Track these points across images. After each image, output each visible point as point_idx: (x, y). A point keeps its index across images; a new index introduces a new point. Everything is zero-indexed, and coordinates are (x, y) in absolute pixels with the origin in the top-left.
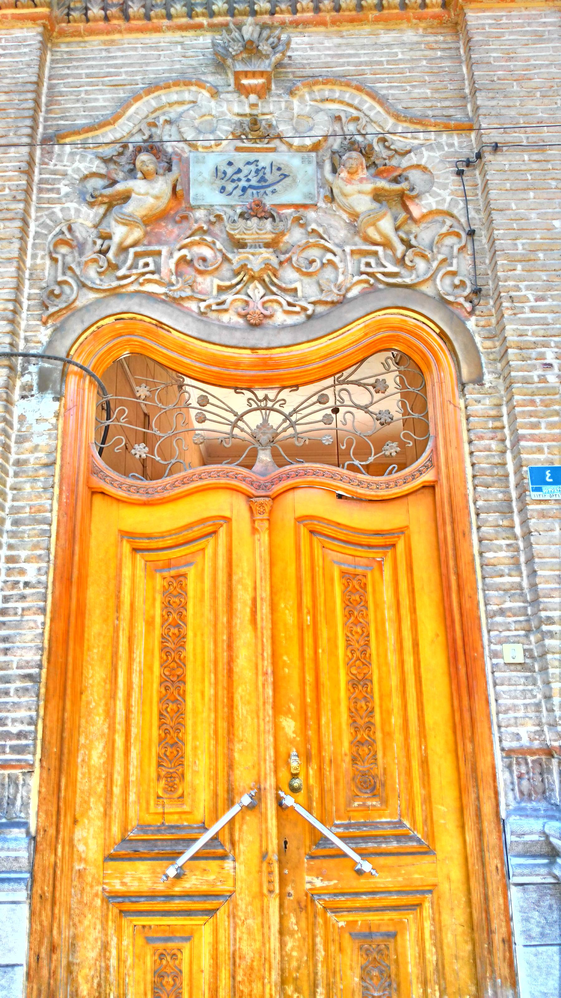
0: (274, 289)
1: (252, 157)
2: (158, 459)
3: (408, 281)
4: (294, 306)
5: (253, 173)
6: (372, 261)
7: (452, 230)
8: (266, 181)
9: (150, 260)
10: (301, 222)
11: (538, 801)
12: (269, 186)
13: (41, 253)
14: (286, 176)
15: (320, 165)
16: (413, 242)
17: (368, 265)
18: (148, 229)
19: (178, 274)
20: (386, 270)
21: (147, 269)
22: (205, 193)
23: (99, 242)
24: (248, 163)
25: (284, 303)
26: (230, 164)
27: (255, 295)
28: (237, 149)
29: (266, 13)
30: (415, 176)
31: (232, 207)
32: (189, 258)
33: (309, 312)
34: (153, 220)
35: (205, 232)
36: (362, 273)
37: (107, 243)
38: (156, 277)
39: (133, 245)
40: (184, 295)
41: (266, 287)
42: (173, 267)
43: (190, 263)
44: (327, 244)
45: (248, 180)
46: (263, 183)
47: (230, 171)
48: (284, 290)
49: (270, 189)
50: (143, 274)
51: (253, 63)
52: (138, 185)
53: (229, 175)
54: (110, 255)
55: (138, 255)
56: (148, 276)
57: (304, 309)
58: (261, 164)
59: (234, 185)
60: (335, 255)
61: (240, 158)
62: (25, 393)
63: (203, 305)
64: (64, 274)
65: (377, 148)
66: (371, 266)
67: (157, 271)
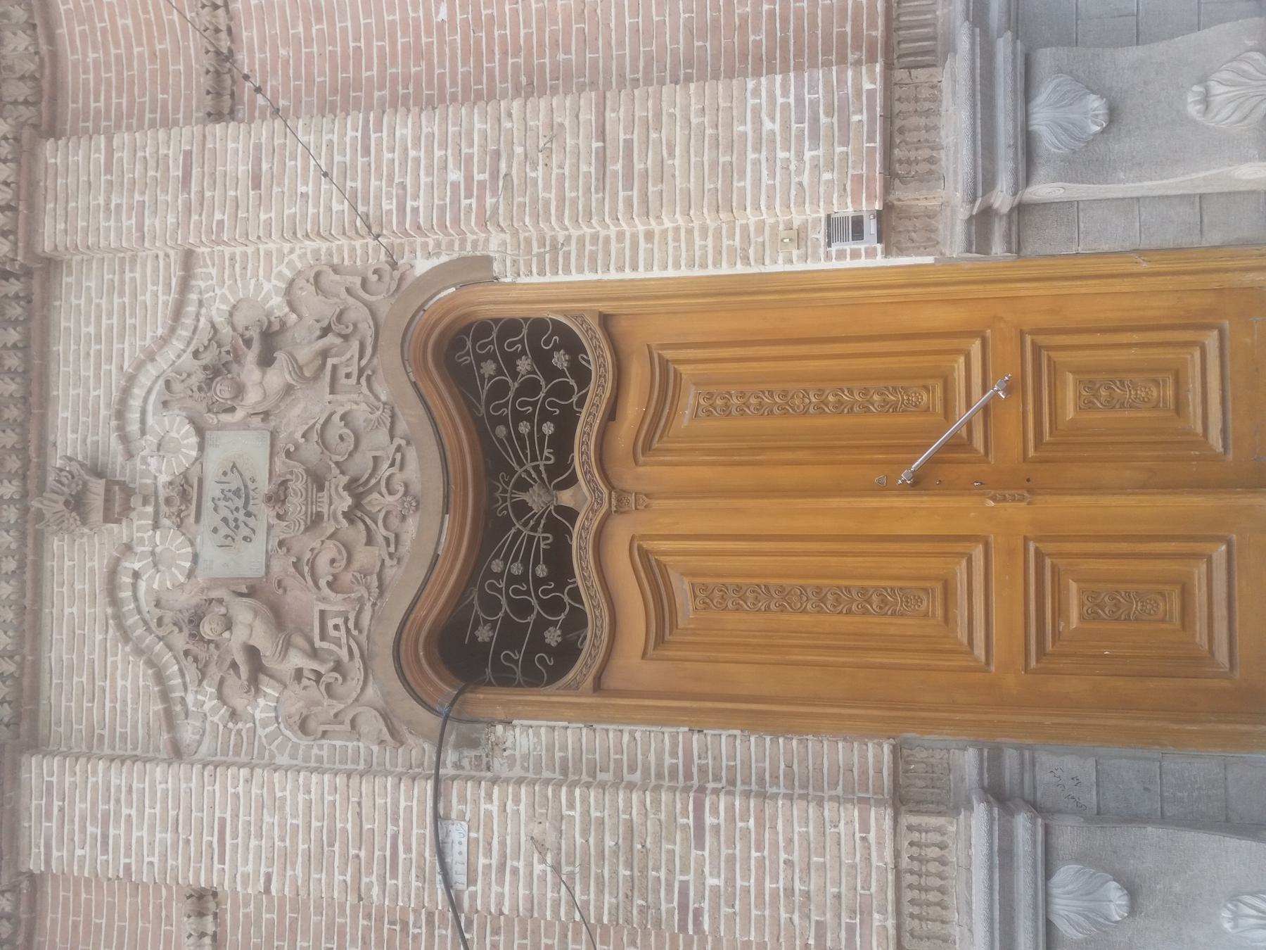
2: (563, 616)
3: (370, 333)
4: (394, 460)
7: (312, 280)
8: (239, 490)
9: (331, 623)
10: (292, 449)
12: (246, 487)
14: (234, 466)
15: (221, 427)
16: (325, 324)
20: (357, 356)
21: (343, 628)
22: (250, 559)
23: (305, 682)
24: (216, 509)
26: (215, 530)
28: (198, 520)
29: (25, 485)
30: (241, 320)
31: (270, 527)
32: (330, 578)
33: (403, 442)
34: (278, 618)
35: (299, 559)
36: (358, 382)
37: (306, 673)
39: (311, 643)
40: (376, 584)
43: (335, 577)
44: (321, 421)
45: (237, 509)
46: (244, 493)
47: (224, 530)
48: (375, 469)
49: (249, 483)
50: (348, 630)
51: (101, 493)
53: (230, 532)
54: (322, 670)
57: (399, 449)
58: (218, 494)
59: (242, 525)
61: (209, 518)
62: (484, 766)
63: (388, 562)
64: (342, 723)
65: (207, 358)
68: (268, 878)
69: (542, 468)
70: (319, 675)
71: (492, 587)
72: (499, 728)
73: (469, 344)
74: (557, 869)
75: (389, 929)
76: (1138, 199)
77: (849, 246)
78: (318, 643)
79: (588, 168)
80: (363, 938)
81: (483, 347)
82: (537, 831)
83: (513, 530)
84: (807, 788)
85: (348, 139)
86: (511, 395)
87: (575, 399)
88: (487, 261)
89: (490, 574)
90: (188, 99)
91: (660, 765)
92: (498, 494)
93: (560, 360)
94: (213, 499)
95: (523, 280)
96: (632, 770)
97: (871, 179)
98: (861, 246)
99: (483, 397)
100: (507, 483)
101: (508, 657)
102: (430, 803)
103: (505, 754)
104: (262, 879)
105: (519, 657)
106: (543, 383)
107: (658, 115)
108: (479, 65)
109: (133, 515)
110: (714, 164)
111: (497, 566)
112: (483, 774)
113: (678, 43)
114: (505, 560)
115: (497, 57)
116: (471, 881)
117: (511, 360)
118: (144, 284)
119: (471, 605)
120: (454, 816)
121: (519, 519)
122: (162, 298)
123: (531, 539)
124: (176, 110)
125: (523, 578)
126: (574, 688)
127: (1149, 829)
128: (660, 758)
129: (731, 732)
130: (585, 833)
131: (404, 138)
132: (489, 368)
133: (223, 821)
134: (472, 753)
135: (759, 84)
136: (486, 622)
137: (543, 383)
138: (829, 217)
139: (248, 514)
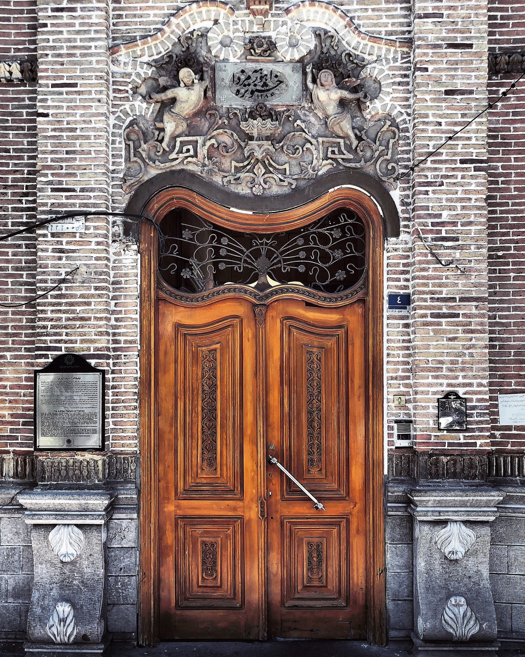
0: (271, 169)
1: (258, 66)
5: (259, 80)
6: (336, 150)
9: (190, 147)
11: (405, 476)
12: (269, 90)
13: (118, 139)
14: (281, 82)
16: (364, 137)
17: (333, 152)
18: (189, 122)
19: (210, 158)
21: (187, 154)
22: (228, 99)
24: (256, 71)
25: (278, 180)
27: (258, 172)
37: (162, 134)
38: (194, 159)
39: (179, 136)
41: (265, 167)
42: (205, 152)
47: (243, 77)
50: (187, 157)
52: (181, 93)
55: (183, 143)
56: (190, 159)
60: (312, 144)
66: (334, 154)
67: (196, 155)
68: (47, 115)
69: (279, 265)
70: (161, 141)
71: (213, 238)
72: (135, 247)
73: (350, 221)
74: (64, 281)
75: (23, 186)
76: (413, 572)
77: (395, 432)
78: (179, 140)
79: (445, 293)
80: (17, 171)
81: (349, 229)
82: (83, 269)
83: (244, 249)
84: (112, 410)
85: (471, 150)
86: (321, 247)
87: (318, 283)
88: (397, 234)
89: (220, 236)
90: (508, 41)
91: (119, 334)
92: (265, 240)
93: (340, 275)
94: (261, 69)
95: (386, 255)
96: (117, 320)
97: (428, 444)
98: (395, 438)
99: (320, 230)
100: (271, 246)
101: (174, 248)
102: (93, 210)
103: (122, 250)
104: (45, 112)
105: (175, 254)
106: (327, 265)
107: (472, 331)
108: (512, 227)
109: (251, 17)
110: (441, 362)
111: (225, 241)
112: (110, 238)
113: (514, 341)
114: (228, 245)
115: (515, 238)
116: (53, 235)
117: (341, 246)
118: (393, 17)
119: (202, 226)
120: (88, 224)
121: (250, 252)
122: (383, 29)
123: (240, 259)
124: (501, 34)
125: (218, 255)
126: (159, 287)
127: (102, 570)
128: (123, 334)
129: (139, 372)
130: (82, 296)
131: (469, 184)
132: (337, 234)
133: (75, 85)
134: (121, 232)
135: (485, 386)
136: (193, 235)
137: (327, 265)
138: (411, 422)
139: (252, 92)
